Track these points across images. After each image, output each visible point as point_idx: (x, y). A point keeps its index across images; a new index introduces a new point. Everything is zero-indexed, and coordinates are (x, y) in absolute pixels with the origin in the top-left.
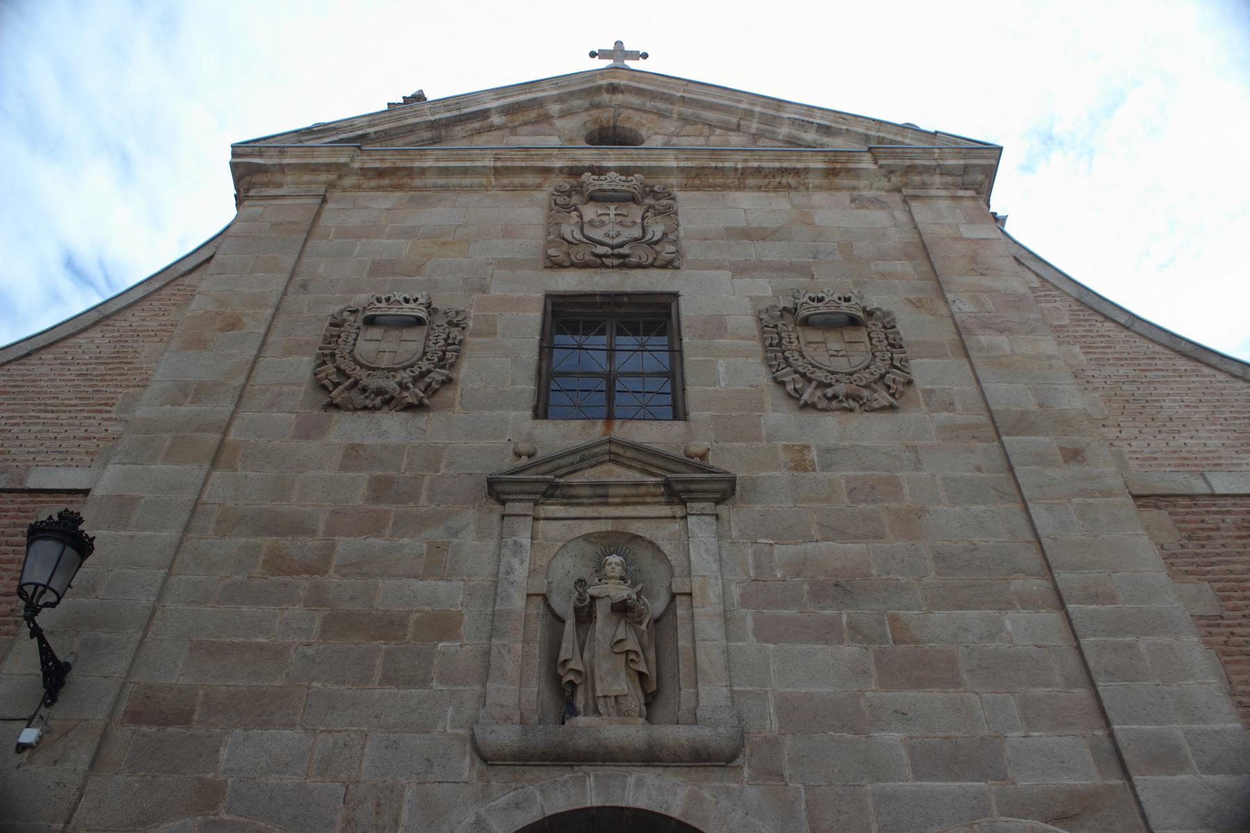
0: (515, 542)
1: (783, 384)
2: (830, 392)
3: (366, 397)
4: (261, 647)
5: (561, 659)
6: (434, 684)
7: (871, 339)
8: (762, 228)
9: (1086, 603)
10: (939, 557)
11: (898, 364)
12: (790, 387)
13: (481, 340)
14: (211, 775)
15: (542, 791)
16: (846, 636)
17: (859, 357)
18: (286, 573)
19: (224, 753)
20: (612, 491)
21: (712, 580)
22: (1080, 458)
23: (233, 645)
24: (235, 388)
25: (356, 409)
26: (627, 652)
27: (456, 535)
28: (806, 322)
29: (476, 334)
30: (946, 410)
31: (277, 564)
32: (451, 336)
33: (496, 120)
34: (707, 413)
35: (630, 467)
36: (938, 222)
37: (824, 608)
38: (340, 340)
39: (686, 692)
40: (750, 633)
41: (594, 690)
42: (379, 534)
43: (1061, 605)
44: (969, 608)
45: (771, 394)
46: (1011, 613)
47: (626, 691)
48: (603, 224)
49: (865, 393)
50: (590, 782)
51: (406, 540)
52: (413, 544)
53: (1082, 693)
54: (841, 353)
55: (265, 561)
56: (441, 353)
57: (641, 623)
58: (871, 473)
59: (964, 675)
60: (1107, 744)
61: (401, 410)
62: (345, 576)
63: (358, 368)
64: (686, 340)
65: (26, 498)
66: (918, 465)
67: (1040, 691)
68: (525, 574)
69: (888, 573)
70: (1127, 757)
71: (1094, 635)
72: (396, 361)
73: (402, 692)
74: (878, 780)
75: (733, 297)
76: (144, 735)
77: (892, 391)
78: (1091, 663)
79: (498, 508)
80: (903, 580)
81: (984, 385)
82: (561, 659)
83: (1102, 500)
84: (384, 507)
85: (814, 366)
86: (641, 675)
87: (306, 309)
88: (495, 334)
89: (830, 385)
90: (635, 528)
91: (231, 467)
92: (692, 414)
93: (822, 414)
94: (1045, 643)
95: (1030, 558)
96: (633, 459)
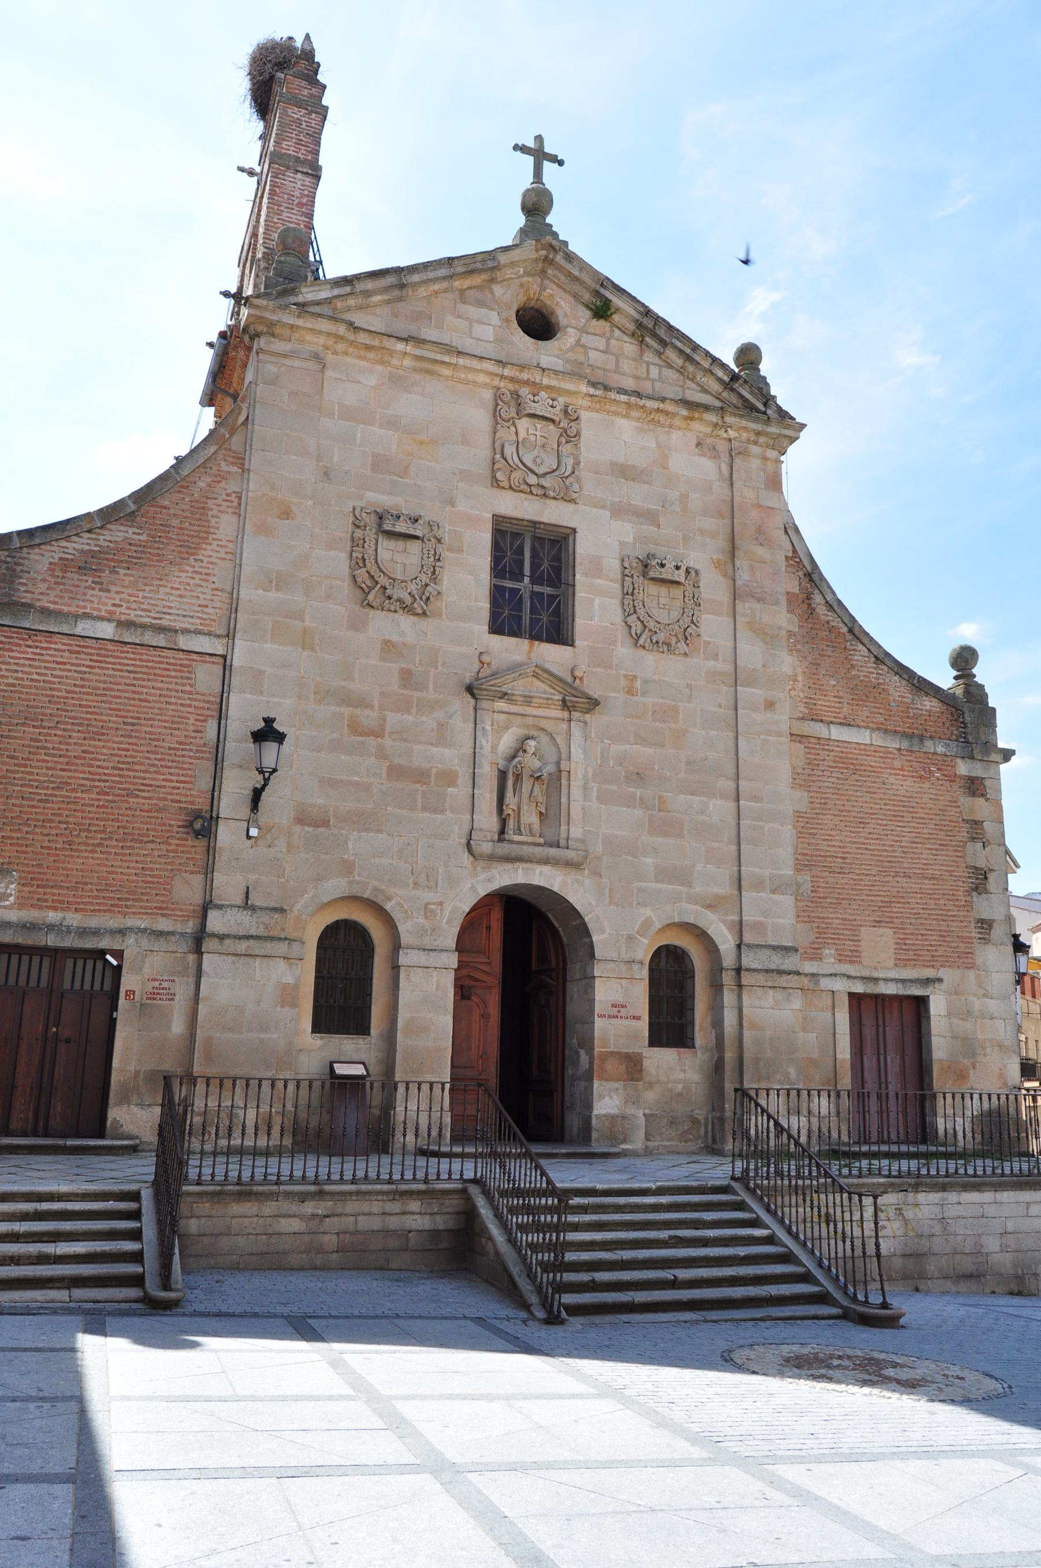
4: (357, 783)
6: (448, 813)
8: (634, 467)
10: (689, 763)
18: (361, 735)
19: (350, 845)
23: (342, 781)
29: (451, 550)
31: (355, 728)
34: (586, 643)
45: (621, 632)
46: (714, 801)
50: (520, 871)
51: (424, 718)
52: (429, 721)
59: (686, 832)
60: (736, 874)
62: (394, 740)
64: (578, 576)
66: (690, 699)
67: (716, 845)
70: (743, 883)
73: (433, 816)
80: (669, 774)
84: (411, 693)
87: (333, 502)
89: (656, 632)
91: (313, 649)
92: (577, 643)
95: (730, 770)
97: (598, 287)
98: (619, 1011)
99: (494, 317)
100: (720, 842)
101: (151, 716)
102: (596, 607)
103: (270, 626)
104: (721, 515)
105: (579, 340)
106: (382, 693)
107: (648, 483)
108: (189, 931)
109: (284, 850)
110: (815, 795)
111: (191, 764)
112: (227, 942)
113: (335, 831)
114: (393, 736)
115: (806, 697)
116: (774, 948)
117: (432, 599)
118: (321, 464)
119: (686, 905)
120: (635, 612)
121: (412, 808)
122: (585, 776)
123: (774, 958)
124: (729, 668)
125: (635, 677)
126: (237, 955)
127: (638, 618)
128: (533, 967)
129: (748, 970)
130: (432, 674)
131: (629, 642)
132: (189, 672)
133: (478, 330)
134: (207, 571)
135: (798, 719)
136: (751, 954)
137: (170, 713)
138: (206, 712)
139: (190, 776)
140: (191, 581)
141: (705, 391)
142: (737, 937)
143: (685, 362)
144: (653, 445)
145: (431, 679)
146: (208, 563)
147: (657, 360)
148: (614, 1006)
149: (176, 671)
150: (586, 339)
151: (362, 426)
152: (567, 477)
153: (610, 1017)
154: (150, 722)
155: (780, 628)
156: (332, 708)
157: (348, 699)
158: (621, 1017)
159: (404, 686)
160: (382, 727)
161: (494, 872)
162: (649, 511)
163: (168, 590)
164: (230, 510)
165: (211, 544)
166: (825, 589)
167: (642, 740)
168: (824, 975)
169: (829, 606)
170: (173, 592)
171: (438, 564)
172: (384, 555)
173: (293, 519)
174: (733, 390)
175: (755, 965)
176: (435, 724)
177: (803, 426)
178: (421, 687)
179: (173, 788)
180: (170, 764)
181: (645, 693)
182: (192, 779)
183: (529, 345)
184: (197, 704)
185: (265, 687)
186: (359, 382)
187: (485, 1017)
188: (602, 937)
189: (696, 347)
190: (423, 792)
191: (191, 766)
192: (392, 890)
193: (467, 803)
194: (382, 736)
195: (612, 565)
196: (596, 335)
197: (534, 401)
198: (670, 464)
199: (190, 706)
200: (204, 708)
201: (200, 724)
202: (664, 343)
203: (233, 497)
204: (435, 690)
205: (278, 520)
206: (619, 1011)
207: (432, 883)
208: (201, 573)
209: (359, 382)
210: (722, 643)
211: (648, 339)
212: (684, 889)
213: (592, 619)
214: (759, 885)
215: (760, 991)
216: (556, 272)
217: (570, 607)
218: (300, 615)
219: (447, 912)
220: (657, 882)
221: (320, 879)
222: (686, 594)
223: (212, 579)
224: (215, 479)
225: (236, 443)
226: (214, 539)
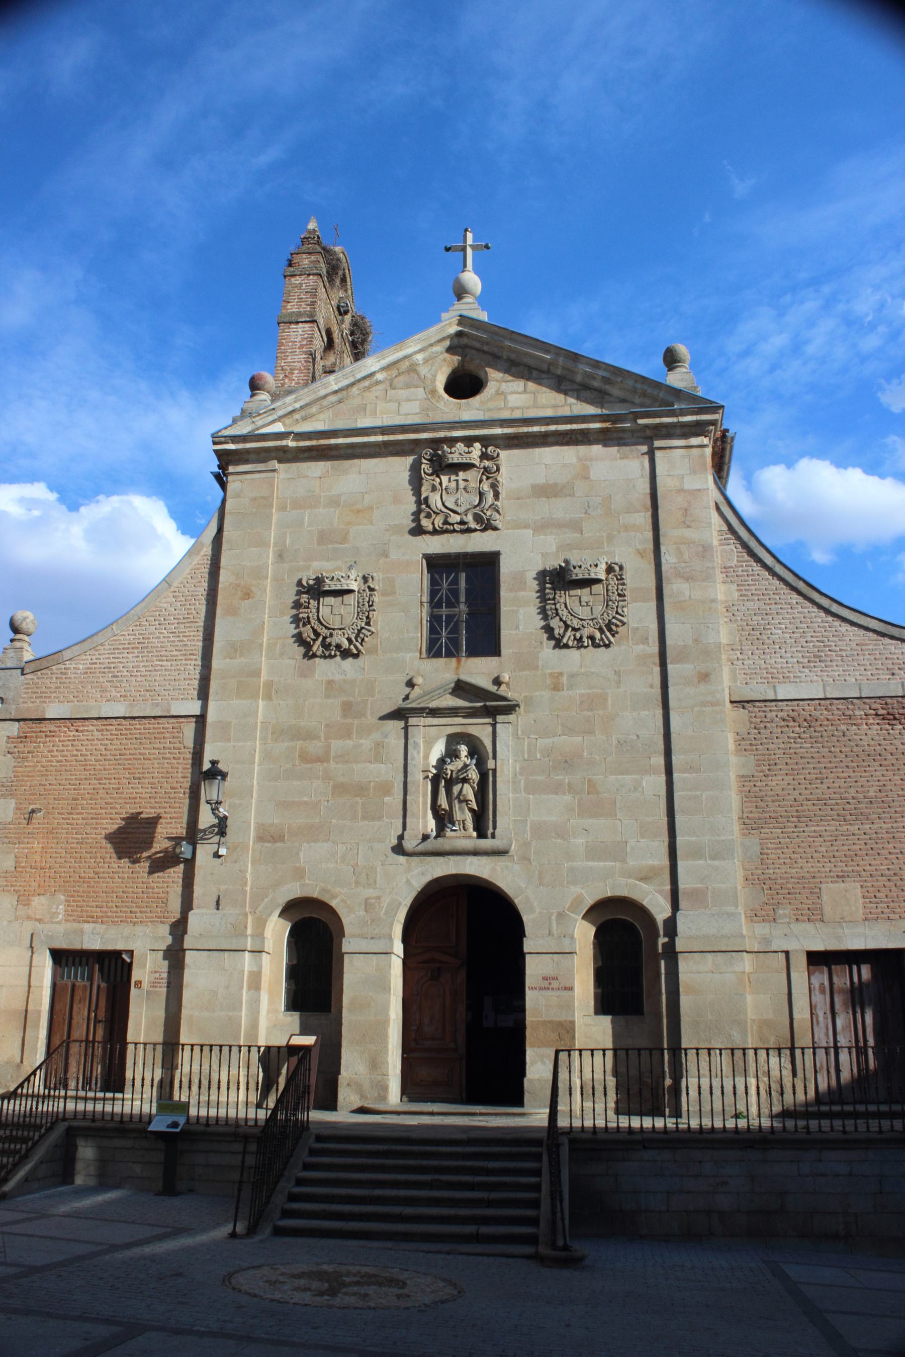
0: (414, 741)
4: (306, 803)
8: (555, 485)
11: (620, 611)
19: (302, 855)
22: (707, 679)
30: (643, 643)
31: (305, 757)
33: (380, 376)
37: (557, 775)
40: (522, 789)
44: (627, 774)
51: (362, 741)
52: (366, 743)
55: (299, 756)
65: (173, 720)
66: (618, 683)
73: (372, 823)
89: (579, 629)
98: (550, 984)
106: (327, 725)
111: (181, 803)
117: (366, 639)
120: (557, 614)
125: (561, 674)
127: (561, 620)
133: (406, 408)
144: (574, 460)
151: (309, 510)
153: (541, 989)
156: (286, 744)
157: (298, 734)
158: (553, 989)
160: (327, 753)
167: (569, 731)
172: (324, 611)
176: (373, 744)
185: (232, 734)
188: (532, 916)
190: (363, 804)
191: (181, 805)
192: (337, 890)
194: (328, 761)
198: (592, 474)
206: (550, 984)
212: (618, 864)
213: (517, 628)
220: (588, 860)
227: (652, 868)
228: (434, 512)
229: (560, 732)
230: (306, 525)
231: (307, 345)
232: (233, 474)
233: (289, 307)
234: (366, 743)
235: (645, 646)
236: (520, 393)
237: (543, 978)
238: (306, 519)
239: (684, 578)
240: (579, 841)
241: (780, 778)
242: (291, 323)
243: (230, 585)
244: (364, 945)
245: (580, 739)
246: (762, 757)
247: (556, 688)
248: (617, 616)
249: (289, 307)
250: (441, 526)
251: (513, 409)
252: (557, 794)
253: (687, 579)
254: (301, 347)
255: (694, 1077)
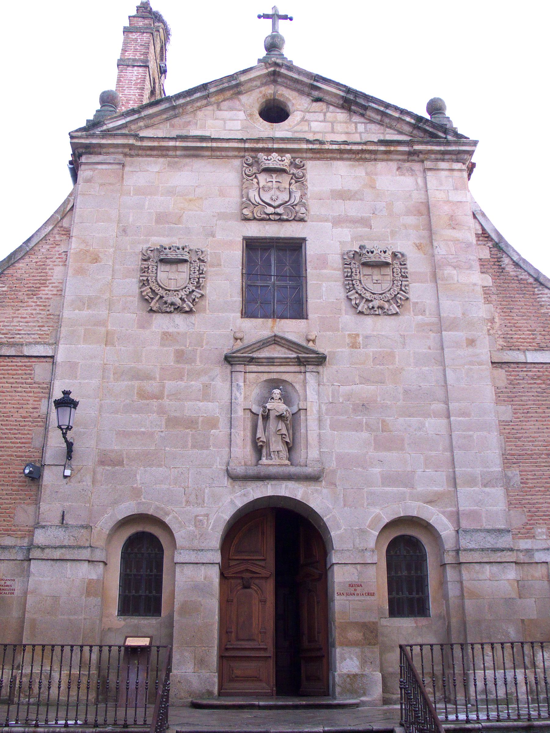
0: (238, 384)
1: (351, 300)
2: (371, 305)
3: (167, 307)
4: (143, 433)
5: (257, 437)
6: (211, 448)
7: (393, 272)
9: (459, 417)
11: (403, 289)
12: (353, 302)
13: (214, 269)
14: (135, 485)
15: (253, 490)
16: (364, 428)
17: (386, 286)
18: (146, 399)
19: (138, 477)
20: (276, 360)
21: (315, 404)
22: (474, 344)
24: (106, 300)
25: (162, 313)
26: (282, 435)
27: (213, 380)
28: (365, 264)
29: (212, 266)
30: (422, 314)
31: (143, 395)
32: (201, 268)
34: (316, 315)
35: (283, 347)
36: (439, 189)
37: (357, 416)
38: (149, 271)
39: (303, 451)
40: (328, 427)
41: (270, 449)
42: (181, 379)
43: (449, 417)
44: (414, 417)
45: (344, 305)
46: (429, 419)
47: (282, 449)
48: (270, 189)
49: (386, 305)
51: (193, 383)
52: (197, 384)
53: (448, 454)
54: (379, 282)
55: (137, 393)
56: (197, 280)
57: (287, 420)
58: (384, 349)
59: (406, 445)
60: (452, 475)
61: (183, 313)
62: (171, 400)
63: (161, 289)
64: (308, 270)
66: (404, 344)
67: (433, 453)
68: (242, 400)
69: (384, 400)
70: (457, 481)
71: (458, 431)
72: (178, 286)
73: (199, 452)
74: (369, 487)
75: (332, 241)
76: (107, 470)
77: (399, 305)
78: (454, 443)
79: (229, 367)
81: (440, 301)
82: (257, 437)
83: (477, 367)
85: (365, 290)
86: (287, 443)
87: (129, 247)
88: (221, 265)
89: (371, 301)
90: (285, 377)
91: (113, 345)
92: (310, 316)
93: (366, 316)
94: (439, 433)
95: (440, 393)
96: (284, 344)
97: (312, 82)
99: (241, 115)
100: (437, 450)
101: (5, 401)
102: (324, 289)
103: (83, 333)
104: (420, 213)
105: (304, 117)
106: (162, 369)
107: (361, 200)
108: (25, 544)
109: (90, 483)
110: (518, 407)
111: (29, 430)
112: (47, 551)
113: (127, 468)
114: (170, 398)
115: (503, 334)
116: (488, 531)
117: (197, 300)
118: (121, 225)
119: (409, 502)
120: (354, 289)
121: (184, 446)
122: (319, 411)
123: (489, 538)
124: (435, 320)
125: (358, 335)
126: (53, 560)
128: (301, 562)
129: (465, 550)
130: (198, 352)
131: (351, 311)
132: (31, 370)
133: (230, 125)
134: (44, 304)
135: (498, 350)
136: (468, 537)
137: (18, 398)
138: (41, 395)
139: (29, 438)
140: (34, 312)
141: (401, 133)
142: (455, 525)
143: (382, 116)
145: (198, 355)
146: (45, 298)
147: (362, 120)
148: (351, 585)
149: (22, 370)
150: (308, 116)
151: (149, 197)
152: (296, 205)
154: (4, 405)
155: (475, 285)
156: (126, 383)
157: (137, 375)
158: (358, 594)
159: (178, 362)
160: (162, 392)
161: (249, 489)
162: (362, 218)
163: (19, 319)
164: (61, 264)
165: (48, 287)
166: (511, 253)
167: (365, 380)
168: (537, 550)
169: (516, 264)
170: (22, 320)
171: (201, 276)
173: (100, 262)
174: (419, 128)
175: (472, 546)
176: (201, 385)
177: (475, 143)
178: (192, 361)
179: (18, 447)
180: (16, 432)
181: (366, 346)
182: (30, 441)
183: (267, 127)
184: (35, 390)
185: (78, 374)
186: (147, 171)
187: (263, 602)
189: (388, 106)
190: (193, 435)
191: (30, 432)
192: (169, 508)
193: (227, 438)
195: (336, 260)
196: (315, 112)
197: (267, 160)
198: (377, 185)
199: (30, 392)
200: (39, 393)
201: (37, 403)
202: (365, 108)
203: (63, 256)
204: (201, 361)
205: (89, 264)
207: (200, 501)
208: (40, 306)
209: (147, 171)
210: (428, 301)
211: (353, 107)
213: (320, 298)
214: (471, 481)
215: (477, 567)
216: (283, 80)
217: (304, 292)
218: (103, 323)
219: (212, 521)
220: (383, 487)
221: (115, 502)
222: (395, 270)
223: (48, 308)
224: (52, 246)
225: (65, 223)
226: (50, 283)
227: (436, 493)
228: (253, 204)
229: (358, 382)
230: (146, 207)
231: (140, 83)
232: (85, 164)
233: (126, 54)
234: (197, 384)
235: (423, 317)
236: (320, 122)
237: (350, 585)
238: (147, 203)
239: (452, 266)
240: (377, 470)
241: (532, 423)
242: (128, 66)
243: (81, 251)
244: (192, 557)
245: (372, 387)
246: (518, 407)
247: (354, 346)
248: (401, 292)
249: (126, 54)
250: (259, 215)
251: (315, 133)
252: (357, 431)
253: (455, 268)
254: (136, 84)
255: (502, 669)
